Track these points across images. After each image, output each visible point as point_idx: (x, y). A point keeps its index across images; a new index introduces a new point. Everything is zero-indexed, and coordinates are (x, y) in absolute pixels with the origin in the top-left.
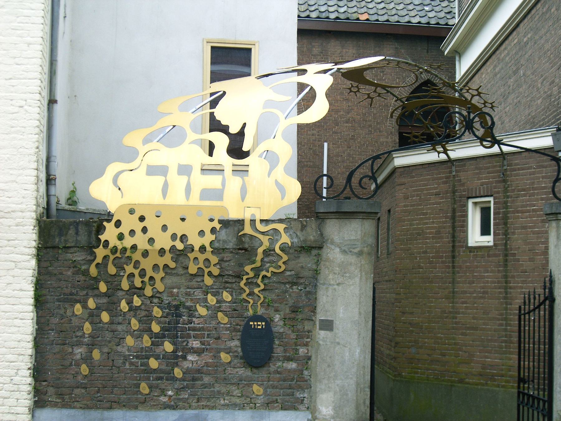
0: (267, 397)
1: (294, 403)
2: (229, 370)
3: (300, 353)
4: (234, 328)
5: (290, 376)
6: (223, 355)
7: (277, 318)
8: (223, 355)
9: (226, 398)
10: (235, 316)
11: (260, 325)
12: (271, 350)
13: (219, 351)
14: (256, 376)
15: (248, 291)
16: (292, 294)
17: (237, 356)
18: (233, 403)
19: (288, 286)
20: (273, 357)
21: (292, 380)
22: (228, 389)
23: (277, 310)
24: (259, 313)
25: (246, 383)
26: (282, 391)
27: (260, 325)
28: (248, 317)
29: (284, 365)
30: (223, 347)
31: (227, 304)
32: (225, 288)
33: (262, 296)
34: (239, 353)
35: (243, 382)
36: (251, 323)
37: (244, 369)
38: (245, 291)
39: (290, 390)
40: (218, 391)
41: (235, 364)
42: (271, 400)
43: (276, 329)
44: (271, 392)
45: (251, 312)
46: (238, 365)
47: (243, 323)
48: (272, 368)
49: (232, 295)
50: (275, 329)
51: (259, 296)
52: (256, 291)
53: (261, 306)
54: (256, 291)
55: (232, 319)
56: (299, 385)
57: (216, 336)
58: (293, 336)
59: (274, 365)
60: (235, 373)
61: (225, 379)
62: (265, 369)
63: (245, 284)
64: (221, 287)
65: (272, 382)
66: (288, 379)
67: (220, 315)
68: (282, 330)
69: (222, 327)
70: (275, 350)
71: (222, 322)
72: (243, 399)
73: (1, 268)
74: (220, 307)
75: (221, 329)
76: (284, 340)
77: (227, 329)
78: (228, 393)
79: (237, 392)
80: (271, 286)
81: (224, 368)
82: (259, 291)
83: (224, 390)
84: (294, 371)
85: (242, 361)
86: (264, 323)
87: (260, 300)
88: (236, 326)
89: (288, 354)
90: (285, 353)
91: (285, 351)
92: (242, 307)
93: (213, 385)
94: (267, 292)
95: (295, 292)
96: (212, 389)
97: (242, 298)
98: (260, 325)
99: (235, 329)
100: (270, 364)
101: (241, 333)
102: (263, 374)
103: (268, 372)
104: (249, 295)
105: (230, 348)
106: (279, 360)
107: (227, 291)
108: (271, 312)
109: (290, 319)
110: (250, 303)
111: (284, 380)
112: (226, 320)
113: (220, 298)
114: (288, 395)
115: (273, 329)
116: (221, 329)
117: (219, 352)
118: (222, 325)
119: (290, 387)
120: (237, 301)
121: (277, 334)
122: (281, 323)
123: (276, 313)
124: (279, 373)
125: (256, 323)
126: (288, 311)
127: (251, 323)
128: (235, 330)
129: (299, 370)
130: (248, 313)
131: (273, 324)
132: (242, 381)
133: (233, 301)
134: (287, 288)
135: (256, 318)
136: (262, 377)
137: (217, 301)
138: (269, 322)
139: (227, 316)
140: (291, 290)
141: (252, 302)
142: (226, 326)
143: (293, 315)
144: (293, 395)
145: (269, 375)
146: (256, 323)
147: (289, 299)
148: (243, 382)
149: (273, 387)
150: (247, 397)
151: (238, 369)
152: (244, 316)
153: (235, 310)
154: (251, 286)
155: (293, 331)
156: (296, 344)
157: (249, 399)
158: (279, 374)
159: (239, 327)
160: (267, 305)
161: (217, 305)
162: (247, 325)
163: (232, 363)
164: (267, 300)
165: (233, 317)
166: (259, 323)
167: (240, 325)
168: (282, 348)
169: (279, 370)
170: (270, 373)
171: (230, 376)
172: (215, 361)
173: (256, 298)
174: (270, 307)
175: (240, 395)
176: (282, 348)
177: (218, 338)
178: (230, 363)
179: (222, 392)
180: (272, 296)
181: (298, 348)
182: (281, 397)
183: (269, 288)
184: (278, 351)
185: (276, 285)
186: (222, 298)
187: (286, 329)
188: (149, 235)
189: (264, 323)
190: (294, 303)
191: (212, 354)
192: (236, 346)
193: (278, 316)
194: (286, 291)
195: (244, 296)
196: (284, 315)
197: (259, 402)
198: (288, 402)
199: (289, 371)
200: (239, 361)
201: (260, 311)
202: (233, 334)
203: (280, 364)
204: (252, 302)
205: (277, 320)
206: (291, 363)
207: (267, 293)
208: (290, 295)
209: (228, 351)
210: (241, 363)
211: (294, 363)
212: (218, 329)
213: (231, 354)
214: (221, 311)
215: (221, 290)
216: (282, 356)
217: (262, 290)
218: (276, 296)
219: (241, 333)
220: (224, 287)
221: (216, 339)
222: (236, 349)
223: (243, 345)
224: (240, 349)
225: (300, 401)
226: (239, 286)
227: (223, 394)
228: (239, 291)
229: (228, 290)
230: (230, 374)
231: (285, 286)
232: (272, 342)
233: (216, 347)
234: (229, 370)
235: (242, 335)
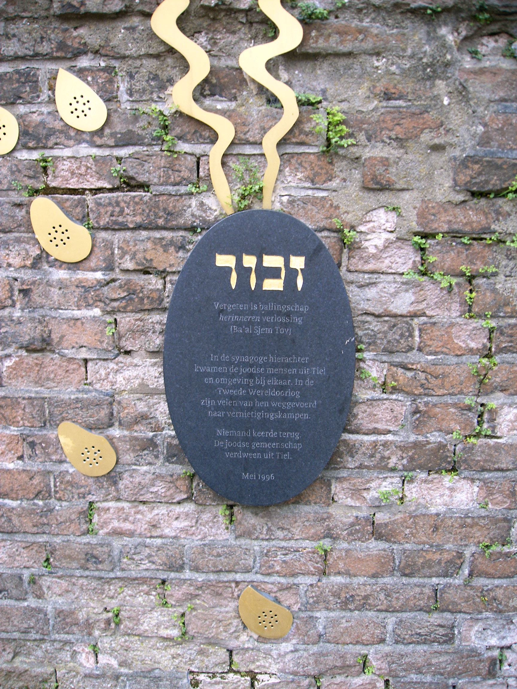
0: (315, 649)
1: (452, 674)
2: (112, 514)
3: (503, 428)
4: (127, 286)
5: (439, 548)
6: (70, 437)
7: (379, 228)
8: (70, 437)
9: (105, 643)
10: (131, 220)
11: (274, 273)
12: (339, 410)
13: (49, 414)
14: (256, 546)
15: (200, 65)
16: (475, 87)
17: (150, 444)
18: (138, 666)
19: (448, 34)
20: (352, 450)
21: (452, 567)
22: (113, 604)
23: (377, 186)
24: (272, 202)
25: (200, 578)
26: (391, 620)
27: (274, 273)
28: (206, 226)
29: (412, 492)
30: (68, 392)
31: (84, 150)
32: (68, 54)
33: (287, 96)
34: (158, 428)
35: (187, 574)
36: (224, 261)
37: (190, 507)
38: (184, 66)
39: (435, 618)
40: (59, 613)
41: (141, 487)
42: (330, 661)
43: (371, 293)
44: (334, 623)
45: (221, 198)
46: (160, 488)
47: (176, 260)
48: (346, 503)
49: (109, 98)
50: (362, 299)
51: (273, 100)
52: (253, 60)
53: (285, 159)
54: (253, 60)
55: (118, 238)
56: (483, 592)
57: (29, 332)
58: (470, 335)
59: (356, 492)
60: (142, 527)
61: (97, 560)
62: (306, 510)
63: (182, 22)
64: (45, 48)
65: (339, 579)
66: (428, 564)
67: (44, 212)
68: (403, 303)
69: (62, 285)
70: (362, 416)
71: (55, 253)
72: (190, 651)
73: (2, 530)
74: (44, 167)
75: (55, 293)
76: (413, 357)
77: (88, 295)
78: (114, 622)
79: (157, 621)
80: (342, 33)
81: (83, 505)
82: (271, 66)
83: (90, 607)
84: (467, 522)
85: (179, 469)
86: (298, 262)
87: (276, 118)
88: (140, 279)
89: (435, 438)
90: (417, 427)
91: (420, 418)
92: (171, 167)
93: (33, 581)
94: (323, 70)
95: (494, 72)
96: (32, 602)
97: (167, 109)
98: (280, 270)
99: (132, 291)
100: (335, 487)
101: (164, 318)
102: (294, 535)
103: (320, 529)
104: (204, 91)
105: (111, 398)
106: (383, 467)
107: (81, 73)
108: (345, 193)
109: (455, 235)
110: (214, 138)
111: (408, 571)
112: (77, 241)
113: (37, 113)
114: (424, 640)
115: (353, 292)
116: (55, 293)
117: (49, 421)
118: (61, 274)
119: (437, 602)
120: (136, 128)
121: (375, 325)
122: (404, 260)
123: (371, 199)
124: (378, 533)
125: (250, 261)
126: (443, 189)
127: (224, 261)
128: (136, 301)
129: (494, 521)
130: (210, 201)
131: (357, 263)
132: (181, 568)
133: (119, 127)
134: (444, 45)
135: (253, 229)
136: (287, 551)
137: (24, 133)
138: (327, 256)
139: (83, 219)
140: (468, 63)
141: (226, 131)
142: (81, 275)
143: (473, 216)
144: (449, 639)
145: (327, 543)
146: (250, 261)
147: (456, 118)
148: (187, 574)
149: (347, 601)
150: (213, 642)
151: (162, 510)
152: (186, 219)
153: (130, 184)
154: (225, 39)
155: (469, 310)
156: (482, 383)
157: (223, 655)
158: (379, 537)
159: (154, 282)
160: (323, 150)
161: (24, 155)
162: (199, 273)
163: (125, 482)
164: (320, 120)
165: (124, 228)
166: (272, 261)
167: (163, 274)
168: (402, 405)
169: (381, 517)
170: (329, 535)
171: (117, 544)
172: (35, 466)
173: (256, 108)
174: (340, 165)
175: (175, 633)
176: (402, 405)
177: (42, 346)
178: (112, 478)
179: (82, 616)
180: (349, 96)
181: (492, 402)
182: (386, 648)
183: (333, 43)
184: (381, 416)
185: (376, 28)
186: (55, 113)
187: (432, 293)
188: (65, 232)
189: (298, 262)
190: (484, 140)
191: (13, 430)
192: (145, 391)
193: (383, 219)
194: (436, 69)
195: (181, 96)
196: (421, 215)
197: (274, 669)
198: (419, 671)
199: (437, 523)
200: (161, 467)
201: (280, 189)
202: (126, 320)
203: (385, 486)
204: (226, 131)
205: (374, 242)
206: (448, 479)
207: (318, 80)
208: (462, 93)
209: (103, 414)
210: (172, 480)
211: (465, 485)
212: (35, 297)
213: (116, 432)
214: (48, 191)
215: (43, 69)
216: (403, 448)
217: (292, 58)
218: (373, 94)
219: (164, 318)
220: (62, 46)
221: (30, 349)
222: (141, 407)
223: (179, 387)
224: (161, 410)
225: (484, 668)
226: (153, 36)
227: (89, 626)
228: (150, 64)
229: (84, 62)
230: (118, 533)
231: (431, 37)
232: (344, 371)
233: (34, 390)
234: (112, 514)
235: (168, 331)
